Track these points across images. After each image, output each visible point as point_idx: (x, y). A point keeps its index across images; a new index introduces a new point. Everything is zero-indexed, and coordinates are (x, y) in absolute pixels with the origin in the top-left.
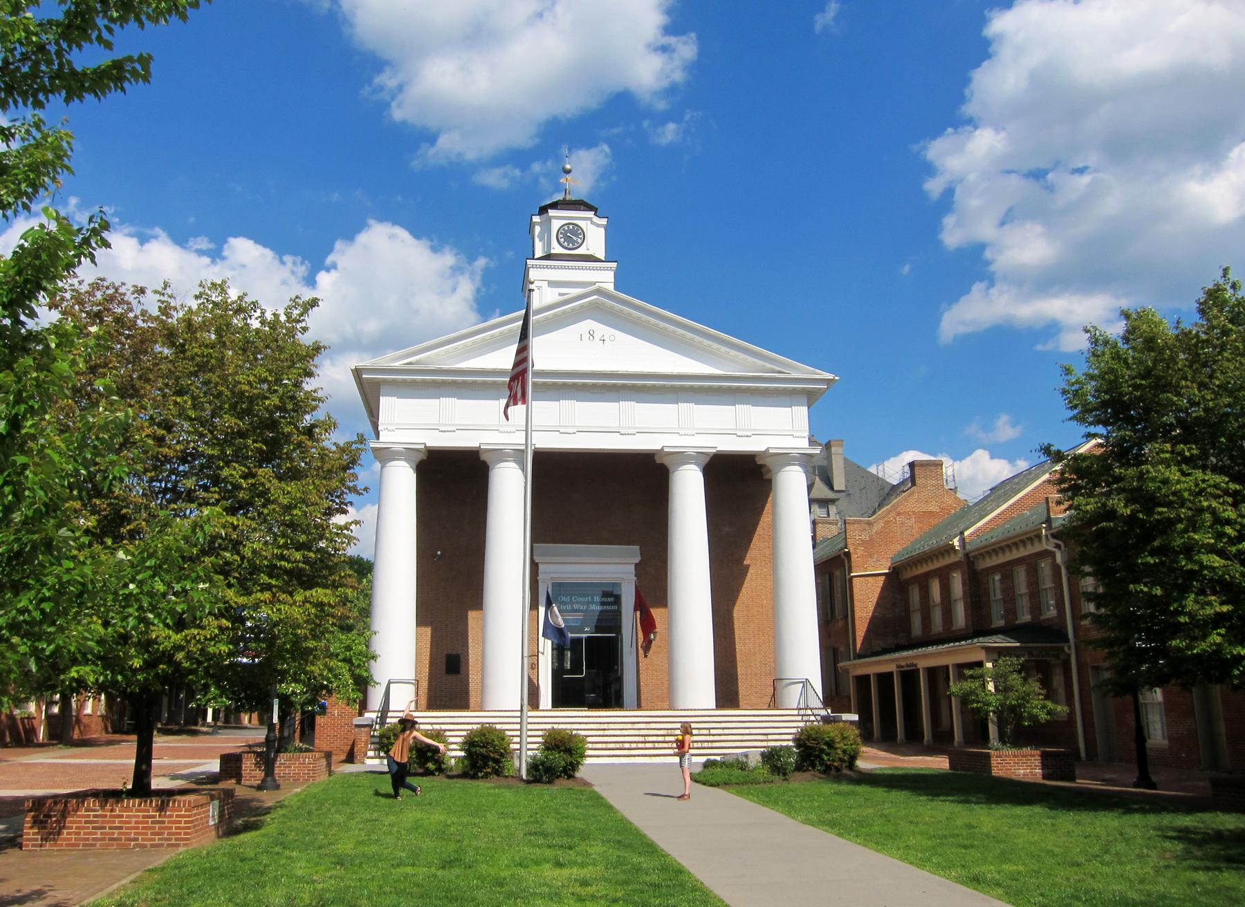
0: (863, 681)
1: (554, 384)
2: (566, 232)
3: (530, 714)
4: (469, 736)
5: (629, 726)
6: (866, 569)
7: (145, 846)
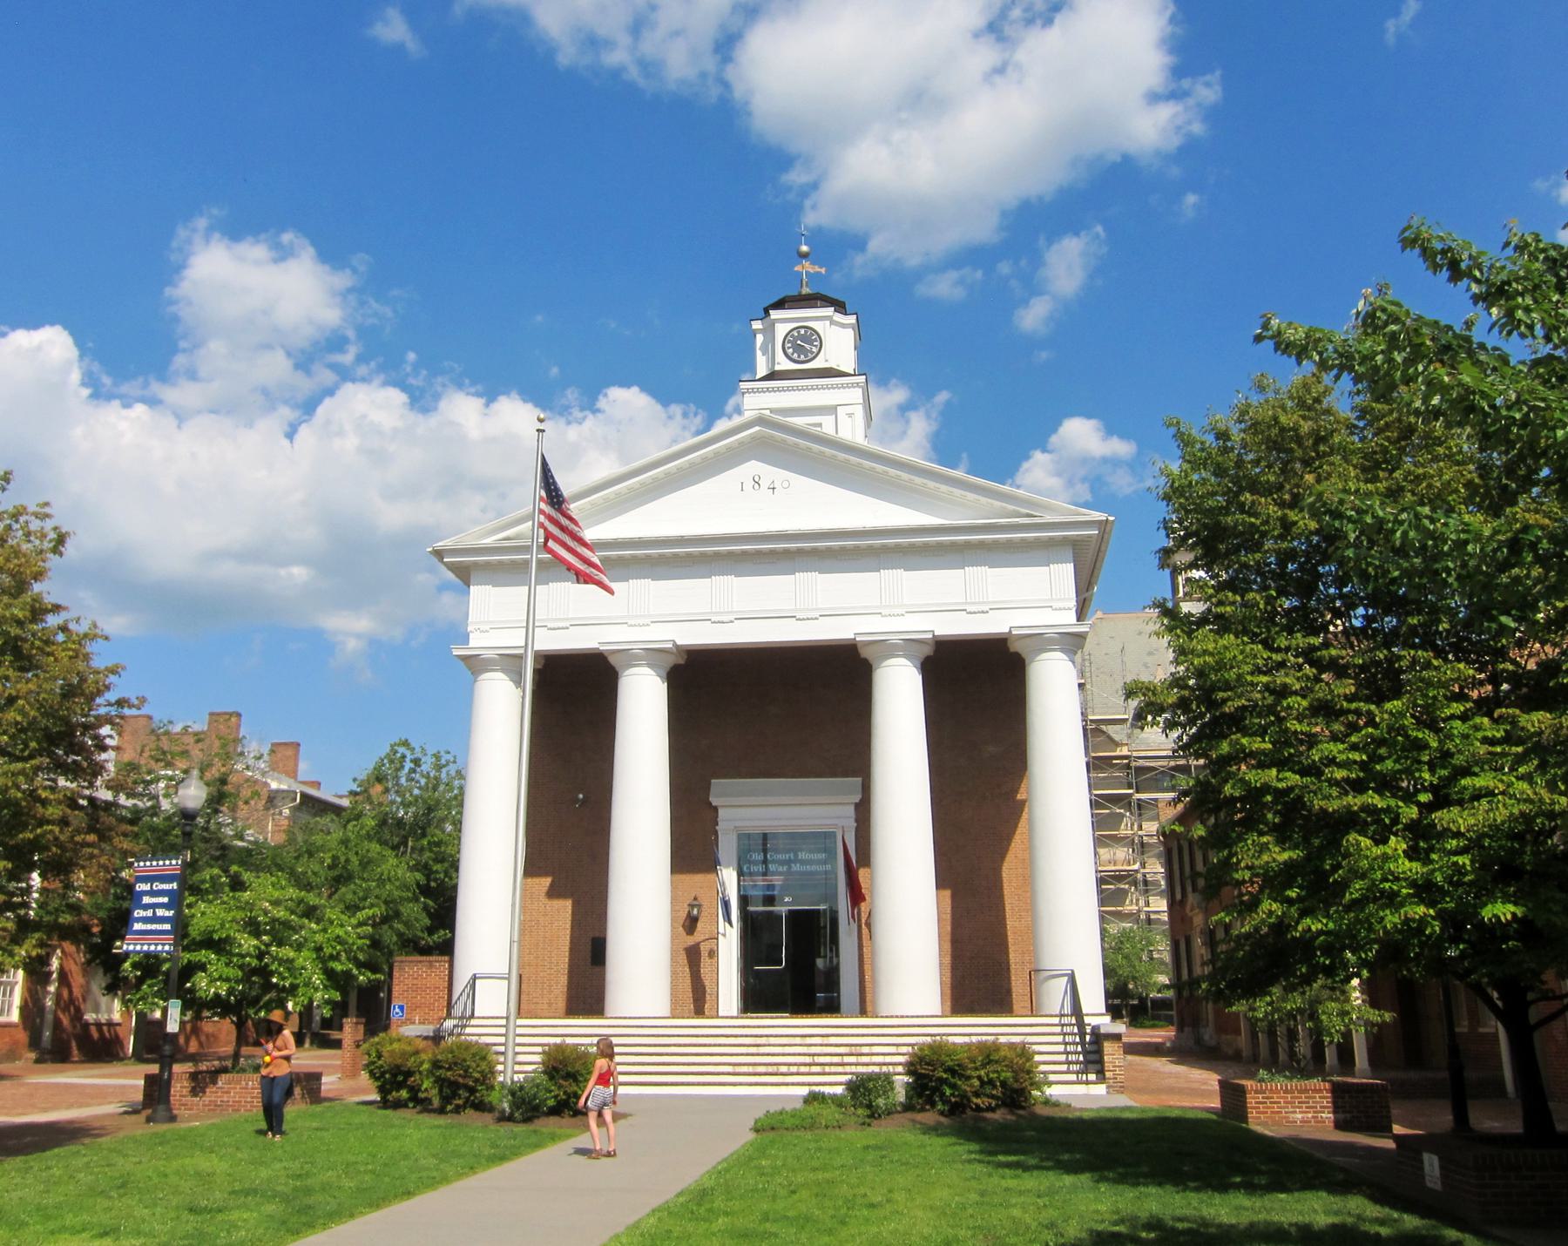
1: (703, 555)
2: (796, 339)
4: (913, 1055)
5: (798, 1041)
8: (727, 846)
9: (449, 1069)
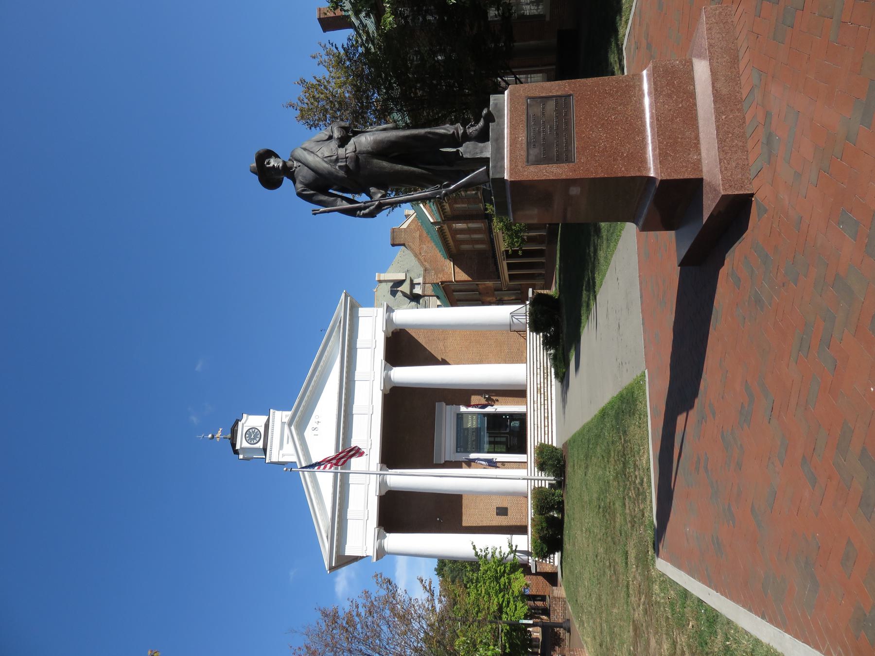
0: (512, 277)
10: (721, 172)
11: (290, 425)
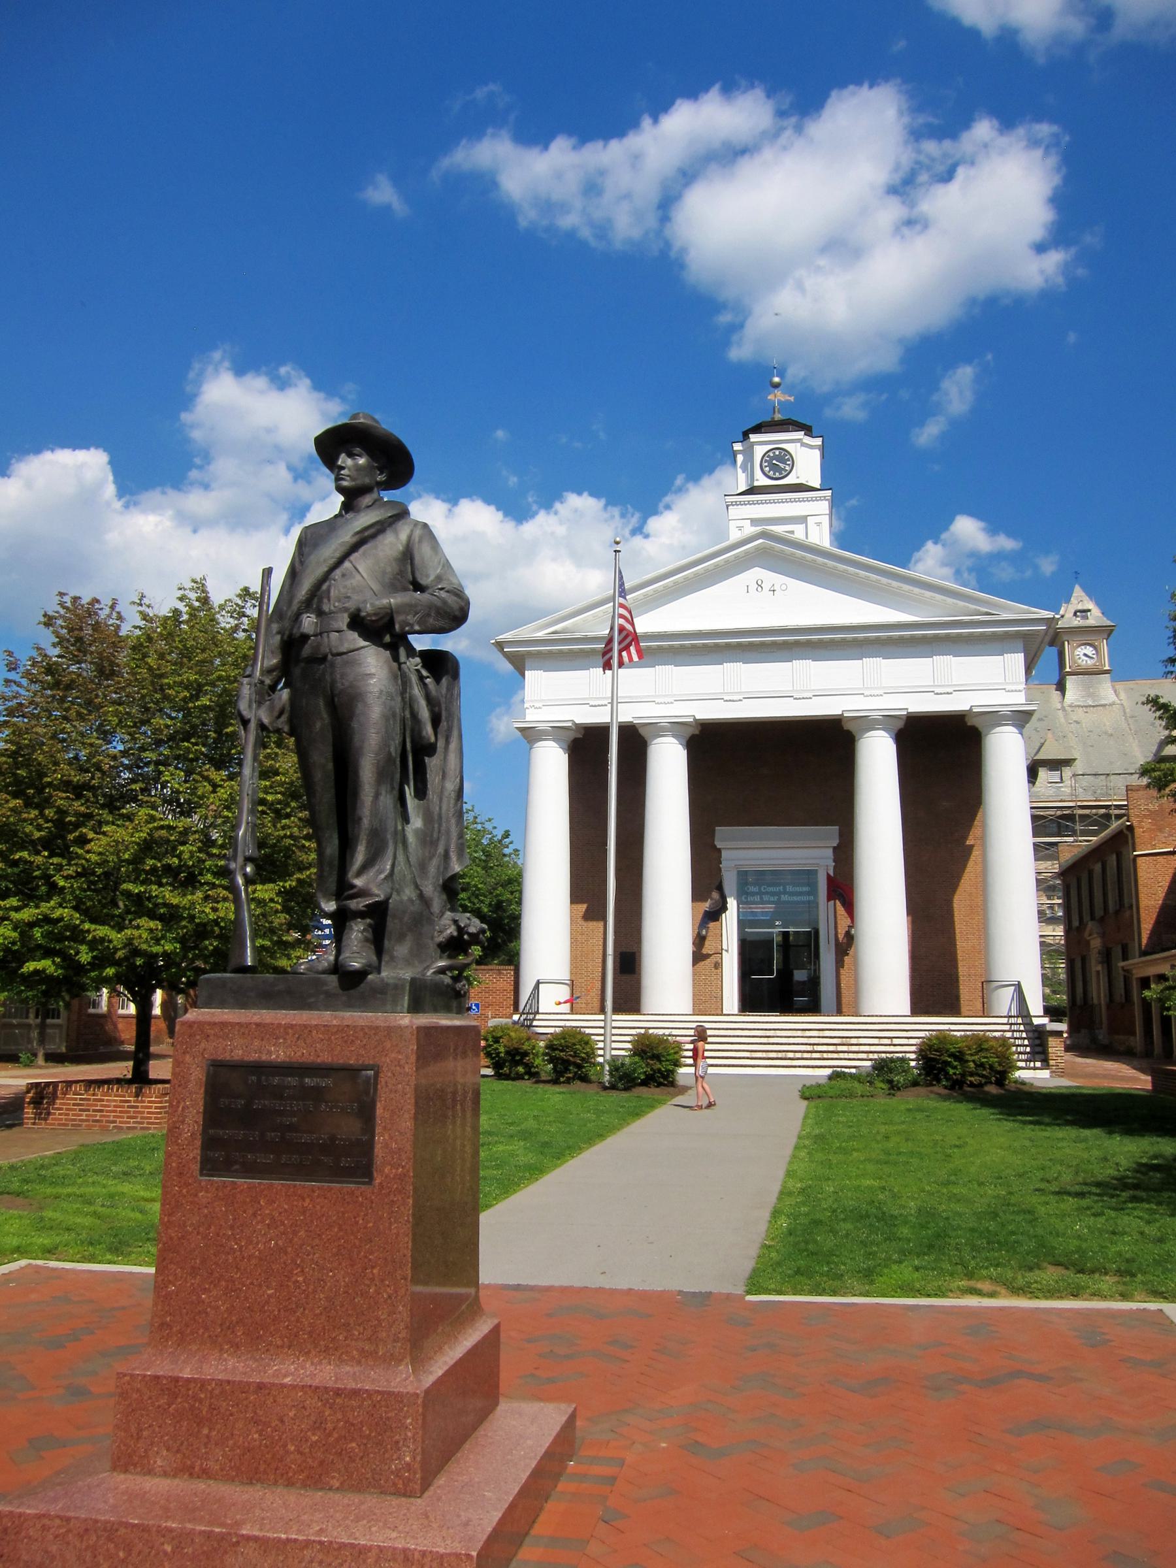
1: (717, 645)
2: (772, 458)
3: (615, 1017)
5: (799, 1033)
6: (1154, 847)
7: (121, 1128)
8: (730, 882)
9: (562, 1051)
10: (39, 1517)
11: (763, 535)
